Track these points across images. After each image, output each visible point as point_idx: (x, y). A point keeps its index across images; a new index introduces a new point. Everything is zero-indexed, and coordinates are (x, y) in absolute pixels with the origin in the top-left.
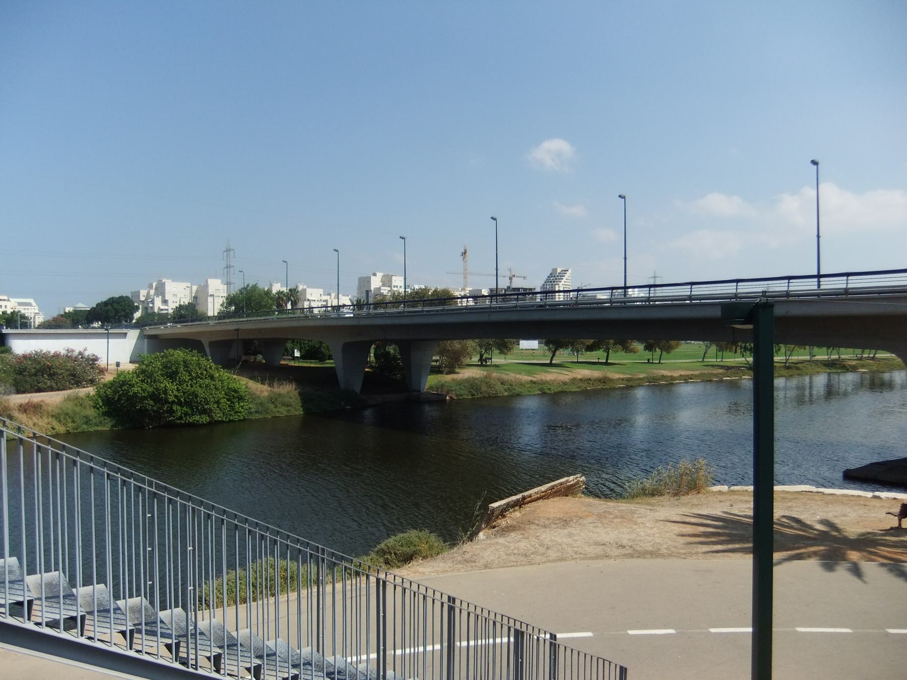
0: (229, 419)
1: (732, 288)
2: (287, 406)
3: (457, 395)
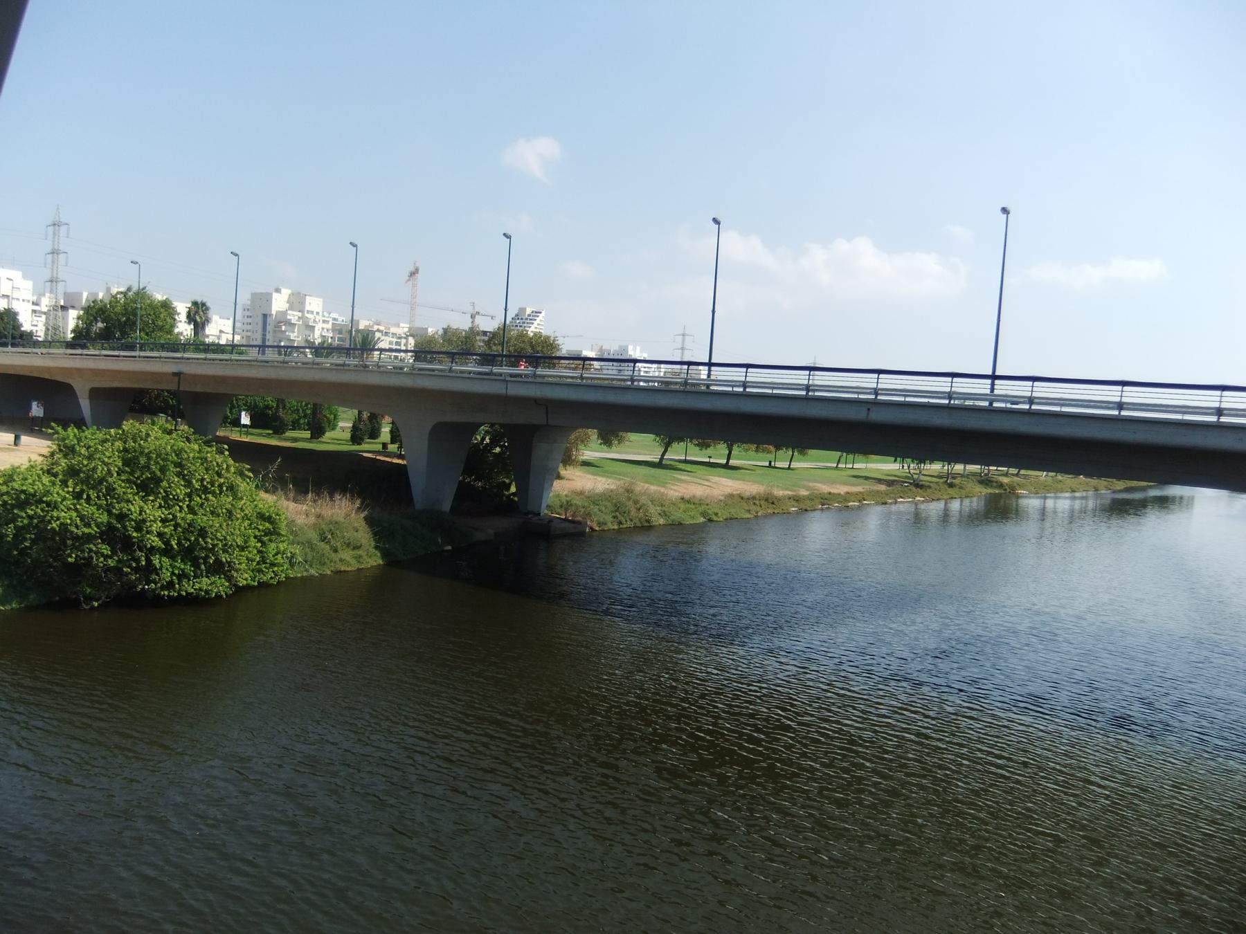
0: (259, 582)
1: (872, 380)
2: (354, 548)
3: (599, 524)
